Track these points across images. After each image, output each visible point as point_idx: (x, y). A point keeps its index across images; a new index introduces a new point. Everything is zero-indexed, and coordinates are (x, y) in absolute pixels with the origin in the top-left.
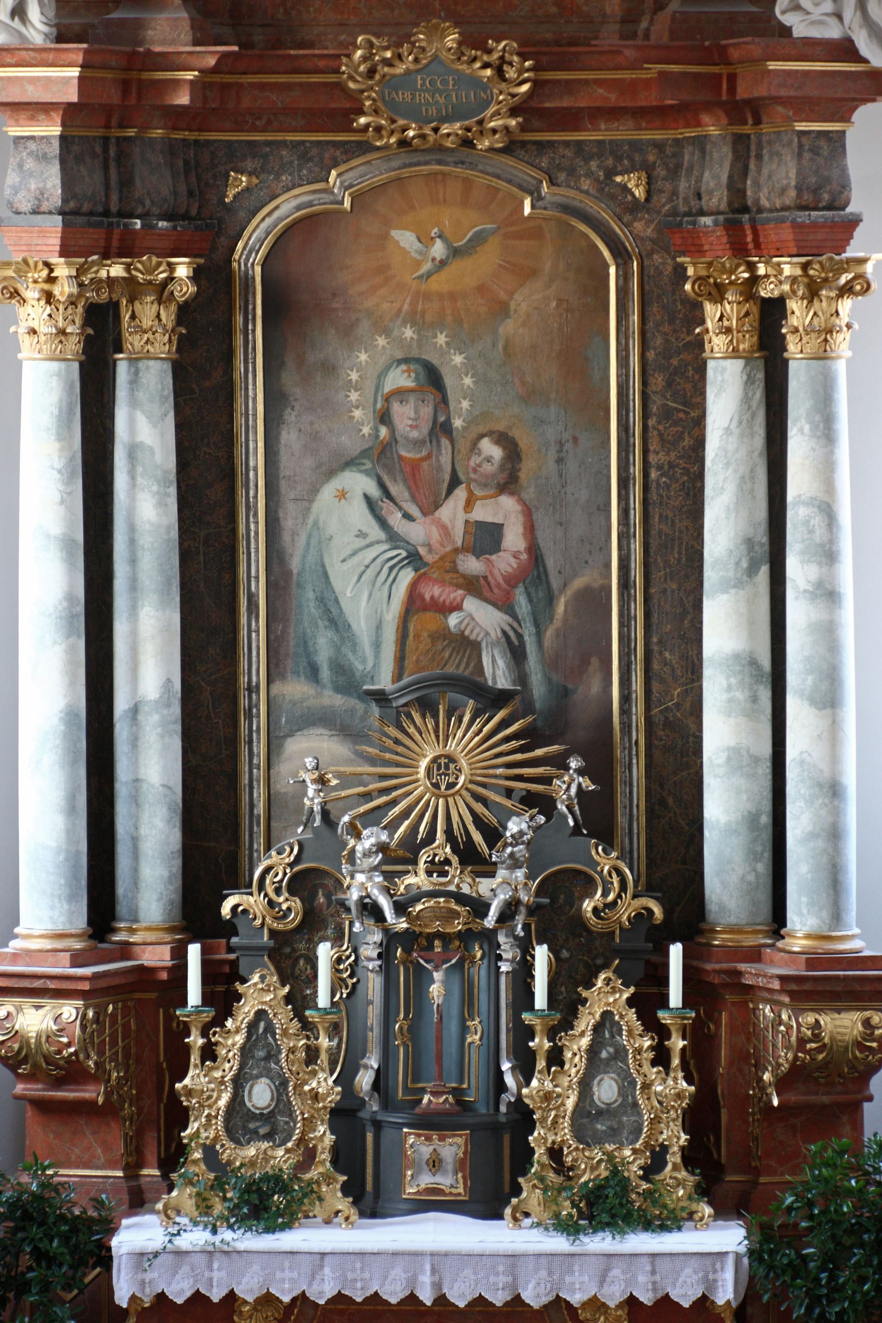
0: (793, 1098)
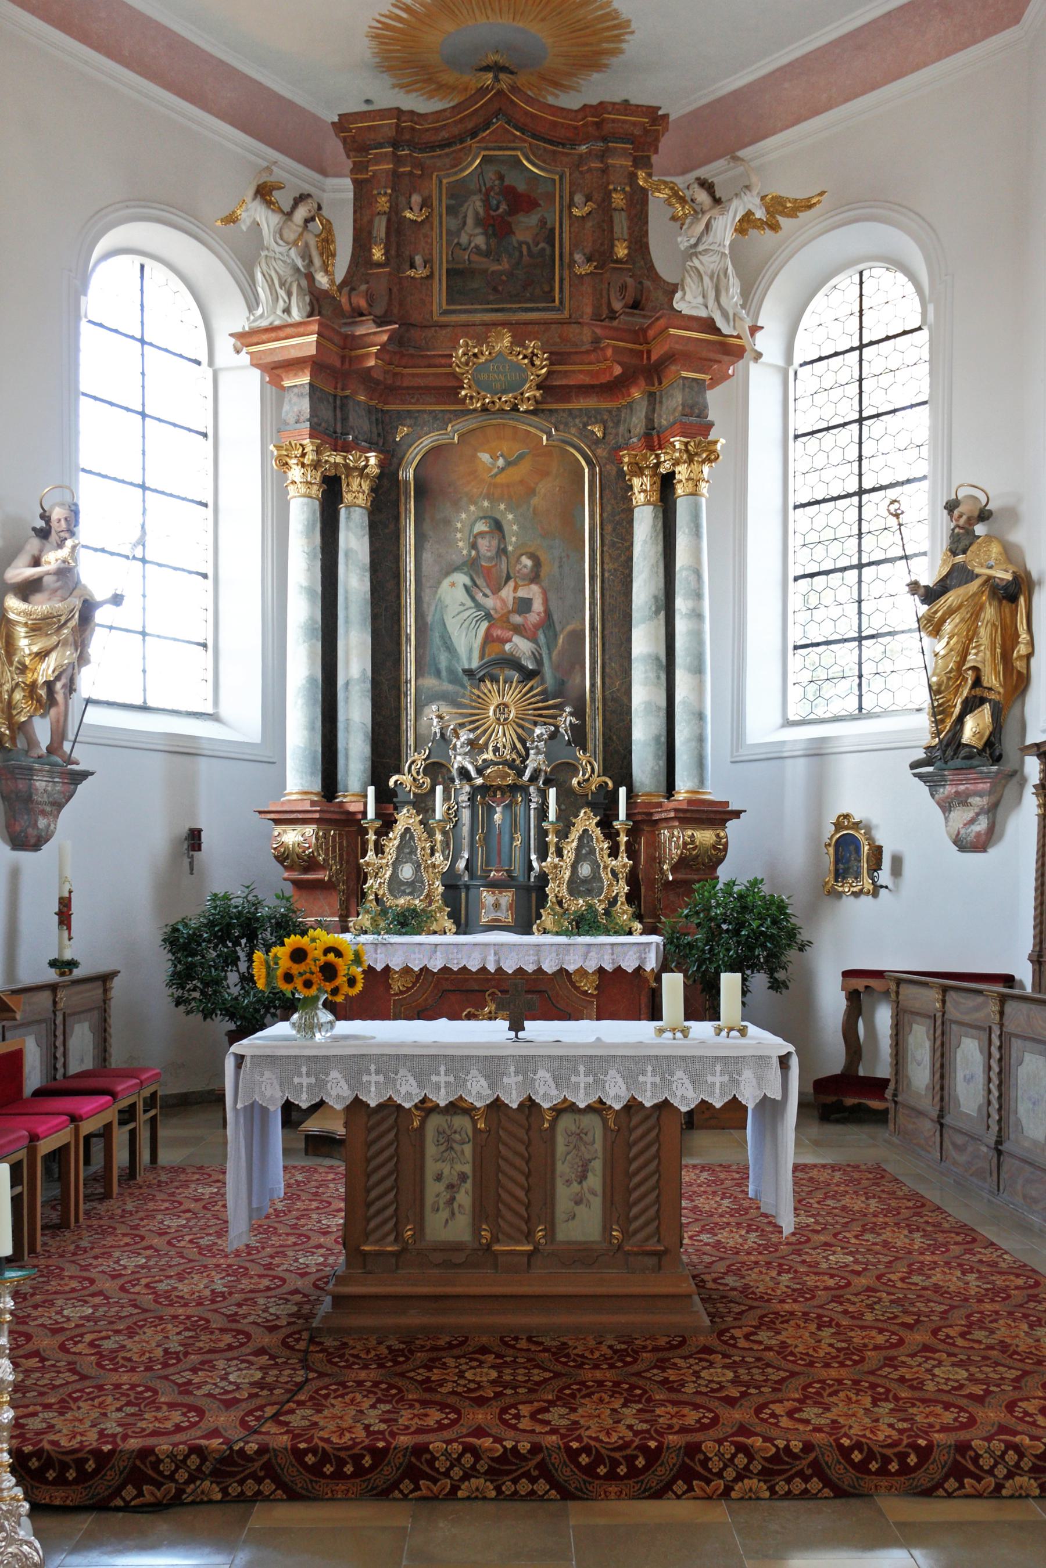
0: (680, 876)
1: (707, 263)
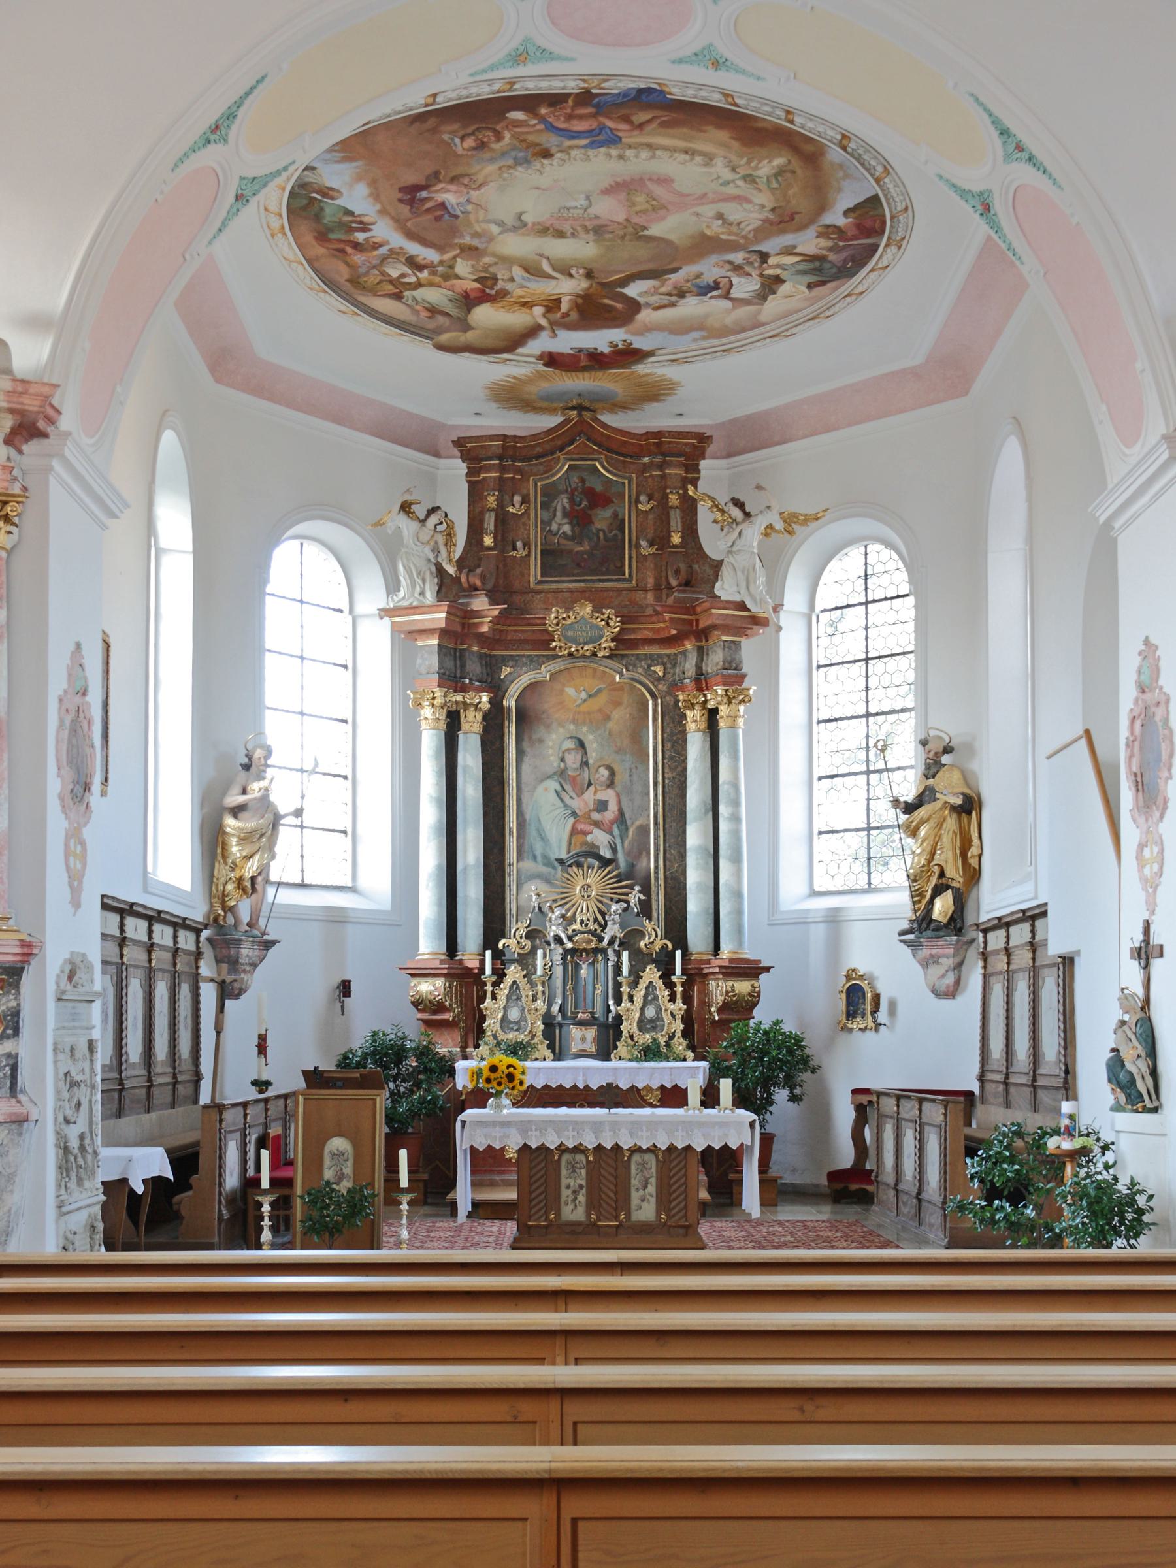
0: (724, 1016)
1: (740, 560)
